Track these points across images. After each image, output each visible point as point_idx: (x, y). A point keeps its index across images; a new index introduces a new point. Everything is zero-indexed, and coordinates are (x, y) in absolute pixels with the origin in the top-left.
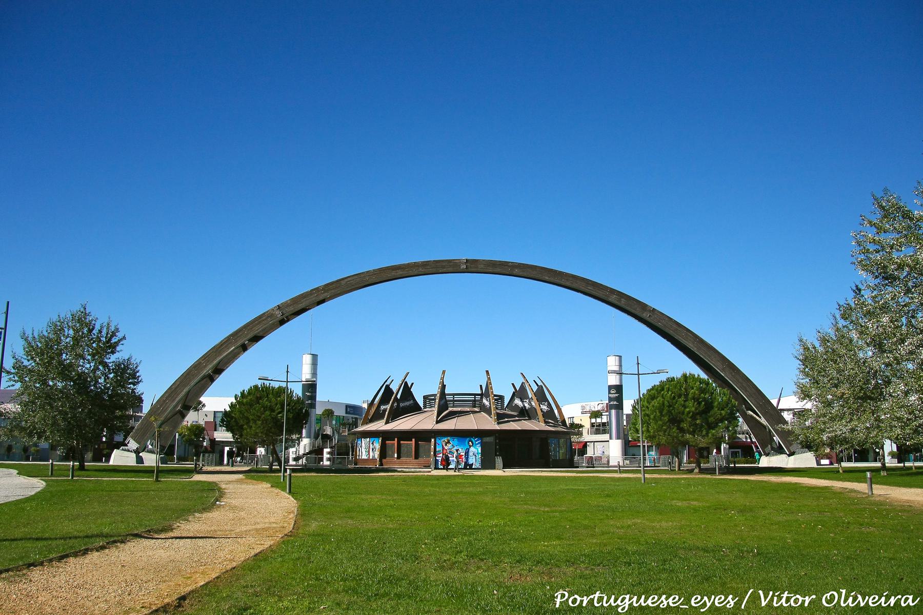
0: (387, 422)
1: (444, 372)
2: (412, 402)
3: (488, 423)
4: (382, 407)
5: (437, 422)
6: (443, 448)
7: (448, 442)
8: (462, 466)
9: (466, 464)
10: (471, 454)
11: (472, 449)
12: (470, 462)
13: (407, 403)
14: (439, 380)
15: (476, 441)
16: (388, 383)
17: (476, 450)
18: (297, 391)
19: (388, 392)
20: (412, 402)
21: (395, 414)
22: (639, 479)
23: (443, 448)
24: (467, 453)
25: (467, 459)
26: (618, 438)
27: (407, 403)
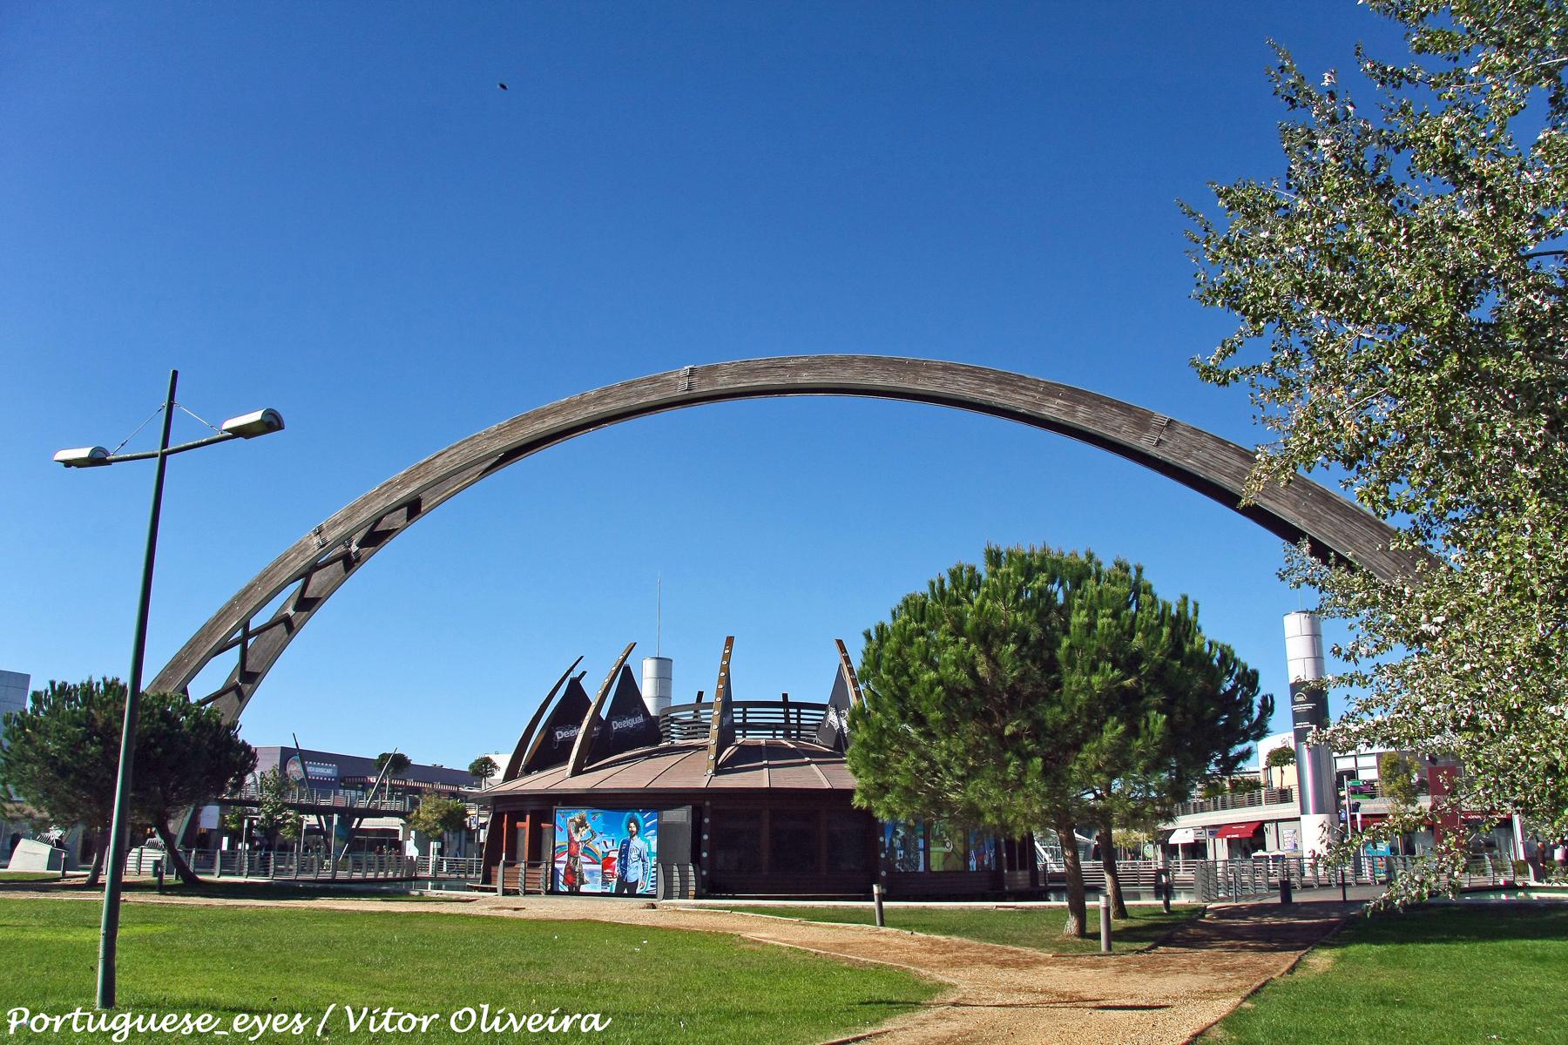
0: (576, 772)
1: (730, 641)
2: (640, 719)
3: (695, 773)
4: (560, 735)
5: (719, 770)
6: (571, 839)
7: (582, 824)
8: (612, 888)
9: (622, 882)
10: (633, 855)
11: (637, 842)
12: (631, 878)
13: (630, 723)
14: (718, 662)
15: (647, 820)
16: (575, 674)
17: (646, 844)
18: (1083, 558)
19: (573, 702)
20: (640, 719)
21: (602, 747)
22: (872, 910)
23: (571, 839)
24: (624, 853)
25: (624, 868)
26: (1320, 810)
27: (630, 723)
